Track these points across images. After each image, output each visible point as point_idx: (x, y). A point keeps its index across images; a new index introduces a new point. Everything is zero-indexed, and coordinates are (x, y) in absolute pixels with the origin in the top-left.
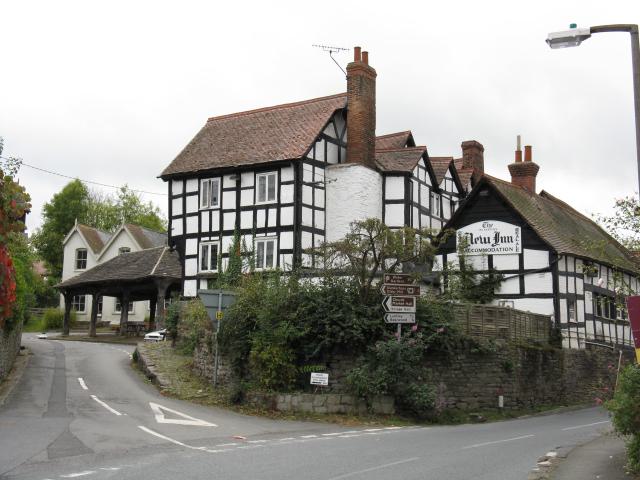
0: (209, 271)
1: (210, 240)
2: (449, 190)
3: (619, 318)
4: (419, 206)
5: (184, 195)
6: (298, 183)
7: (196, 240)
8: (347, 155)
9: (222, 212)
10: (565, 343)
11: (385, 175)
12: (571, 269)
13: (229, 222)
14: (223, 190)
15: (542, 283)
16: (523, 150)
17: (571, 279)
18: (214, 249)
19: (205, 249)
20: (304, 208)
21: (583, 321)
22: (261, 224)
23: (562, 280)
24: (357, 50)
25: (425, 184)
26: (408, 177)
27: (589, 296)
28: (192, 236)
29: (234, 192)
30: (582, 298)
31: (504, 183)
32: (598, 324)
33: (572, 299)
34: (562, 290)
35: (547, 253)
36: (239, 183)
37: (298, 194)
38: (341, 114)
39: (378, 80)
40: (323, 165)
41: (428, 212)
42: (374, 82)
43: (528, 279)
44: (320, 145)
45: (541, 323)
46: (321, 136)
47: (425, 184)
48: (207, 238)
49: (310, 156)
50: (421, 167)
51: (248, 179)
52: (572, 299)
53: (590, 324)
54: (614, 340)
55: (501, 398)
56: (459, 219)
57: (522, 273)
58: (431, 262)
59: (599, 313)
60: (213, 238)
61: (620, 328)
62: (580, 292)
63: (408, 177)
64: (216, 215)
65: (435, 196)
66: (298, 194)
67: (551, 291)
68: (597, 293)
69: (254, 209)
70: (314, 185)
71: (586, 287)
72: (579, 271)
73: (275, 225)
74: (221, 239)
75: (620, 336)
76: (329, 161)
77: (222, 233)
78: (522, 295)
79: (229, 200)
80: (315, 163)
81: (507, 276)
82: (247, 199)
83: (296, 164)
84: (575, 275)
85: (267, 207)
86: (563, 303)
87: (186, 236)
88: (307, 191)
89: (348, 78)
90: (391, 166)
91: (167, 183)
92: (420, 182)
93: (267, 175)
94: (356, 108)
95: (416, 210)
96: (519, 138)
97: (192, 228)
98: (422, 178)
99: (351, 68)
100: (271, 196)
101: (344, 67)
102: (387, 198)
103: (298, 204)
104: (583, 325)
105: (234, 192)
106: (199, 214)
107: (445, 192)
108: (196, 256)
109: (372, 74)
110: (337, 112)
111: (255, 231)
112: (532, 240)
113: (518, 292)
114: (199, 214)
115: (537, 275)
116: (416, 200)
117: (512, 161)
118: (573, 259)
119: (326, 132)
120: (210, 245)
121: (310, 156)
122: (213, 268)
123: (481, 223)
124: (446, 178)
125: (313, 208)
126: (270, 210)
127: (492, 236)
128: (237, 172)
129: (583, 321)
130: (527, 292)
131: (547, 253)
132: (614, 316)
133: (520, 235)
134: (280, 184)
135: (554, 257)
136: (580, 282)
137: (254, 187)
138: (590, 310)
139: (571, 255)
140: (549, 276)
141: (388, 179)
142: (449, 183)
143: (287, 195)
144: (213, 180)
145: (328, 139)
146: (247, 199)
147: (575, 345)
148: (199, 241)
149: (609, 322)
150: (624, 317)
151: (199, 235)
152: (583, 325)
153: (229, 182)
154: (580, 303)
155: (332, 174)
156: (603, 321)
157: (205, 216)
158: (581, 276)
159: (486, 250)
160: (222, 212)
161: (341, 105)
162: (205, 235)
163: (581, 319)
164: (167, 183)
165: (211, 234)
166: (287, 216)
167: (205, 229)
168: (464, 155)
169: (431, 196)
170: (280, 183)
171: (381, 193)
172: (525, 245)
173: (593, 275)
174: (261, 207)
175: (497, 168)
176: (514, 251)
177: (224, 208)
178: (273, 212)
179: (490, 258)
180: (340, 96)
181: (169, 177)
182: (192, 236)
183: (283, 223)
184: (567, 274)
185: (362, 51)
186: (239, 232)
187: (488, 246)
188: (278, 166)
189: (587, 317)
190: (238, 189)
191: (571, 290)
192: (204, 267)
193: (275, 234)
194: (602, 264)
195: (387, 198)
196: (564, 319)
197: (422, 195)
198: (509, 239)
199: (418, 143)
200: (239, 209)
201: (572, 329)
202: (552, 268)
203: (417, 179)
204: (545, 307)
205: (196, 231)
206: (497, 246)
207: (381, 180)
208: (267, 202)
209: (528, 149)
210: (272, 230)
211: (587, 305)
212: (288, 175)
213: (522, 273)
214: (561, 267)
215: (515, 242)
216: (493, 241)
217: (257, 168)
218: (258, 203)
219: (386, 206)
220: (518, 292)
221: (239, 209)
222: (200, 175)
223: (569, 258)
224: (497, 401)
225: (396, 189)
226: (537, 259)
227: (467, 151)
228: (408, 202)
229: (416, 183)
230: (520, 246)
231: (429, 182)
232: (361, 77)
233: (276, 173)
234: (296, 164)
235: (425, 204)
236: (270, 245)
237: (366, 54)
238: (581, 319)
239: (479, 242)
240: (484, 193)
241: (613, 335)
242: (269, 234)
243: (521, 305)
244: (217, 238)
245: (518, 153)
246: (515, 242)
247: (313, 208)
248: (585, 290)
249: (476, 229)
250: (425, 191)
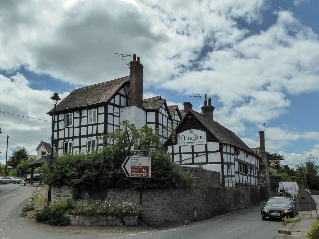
1: (69, 141)
3: (249, 173)
5: (58, 121)
8: (130, 103)
9: (74, 128)
10: (226, 185)
11: (147, 111)
12: (229, 151)
13: (77, 133)
14: (74, 118)
15: (216, 157)
17: (229, 156)
21: (236, 175)
22: (90, 133)
23: (225, 156)
24: (134, 56)
25: (165, 116)
26: (157, 112)
27: (236, 163)
28: (61, 139)
30: (234, 164)
31: (199, 114)
32: (241, 176)
33: (229, 165)
34: (225, 160)
35: (218, 143)
36: (81, 114)
40: (119, 107)
43: (209, 155)
44: (117, 97)
45: (215, 175)
46: (117, 93)
47: (165, 116)
48: (67, 140)
49: (112, 102)
51: (84, 113)
52: (229, 165)
53: (237, 176)
54: (247, 183)
56: (180, 129)
57: (206, 153)
59: (241, 171)
60: (70, 140)
61: (249, 177)
62: (233, 161)
63: (157, 112)
64: (71, 129)
68: (240, 163)
69: (87, 126)
71: (235, 160)
72: (233, 151)
74: (73, 140)
75: (249, 181)
77: (73, 137)
78: (207, 163)
79: (77, 123)
80: (114, 105)
81: (199, 154)
84: (231, 154)
85: (92, 125)
86: (225, 166)
87: (59, 139)
88: (110, 118)
90: (150, 108)
92: (163, 115)
93: (92, 110)
95: (160, 127)
97: (61, 136)
98: (164, 113)
99: (131, 63)
100: (94, 120)
103: (106, 123)
104: (234, 176)
106: (64, 129)
107: (174, 120)
110: (125, 83)
111: (87, 136)
112: (211, 138)
114: (64, 129)
117: (203, 105)
118: (252, 177)
119: (120, 92)
121: (112, 102)
128: (80, 110)
129: (236, 175)
131: (218, 143)
133: (206, 136)
134: (98, 114)
135: (221, 145)
136: (232, 157)
137: (87, 116)
138: (237, 170)
139: (229, 145)
140: (219, 153)
141: (148, 113)
143: (101, 119)
144: (70, 114)
145: (121, 95)
147: (231, 185)
148: (64, 141)
149: (245, 175)
150: (250, 173)
151: (64, 139)
152: (234, 176)
153: (77, 115)
154: (233, 166)
155: (122, 110)
157: (67, 130)
158: (233, 155)
160: (74, 128)
161: (127, 80)
163: (233, 174)
165: (69, 138)
166: (101, 129)
167: (67, 136)
172: (208, 140)
173: (237, 154)
174: (90, 125)
175: (198, 109)
176: (203, 143)
178: (95, 127)
179: (193, 146)
180: (127, 77)
181: (51, 113)
182: (61, 139)
184: (227, 153)
186: (80, 137)
187: (192, 141)
188: (97, 106)
189: (236, 173)
190: (80, 118)
191: (229, 161)
196: (226, 174)
197: (164, 120)
198: (201, 138)
200: (81, 126)
201: (229, 178)
202: (221, 150)
203: (161, 113)
204: (217, 168)
205: (220, 165)
206: (196, 141)
208: (93, 123)
210: (95, 135)
211: (235, 168)
212: (101, 110)
213: (206, 153)
214: (224, 150)
215: (203, 139)
216: (193, 139)
221: (81, 126)
222: (65, 112)
224: (194, 213)
226: (213, 146)
227: (185, 106)
228: (157, 123)
229: (160, 115)
230: (206, 141)
231: (167, 115)
234: (105, 105)
235: (165, 124)
237: (138, 58)
238: (233, 174)
239: (187, 139)
241: (247, 181)
242: (93, 137)
243: (206, 167)
244: (72, 140)
245: (206, 102)
246: (203, 139)
247: (114, 125)
248: (235, 161)
249: (187, 133)
250: (165, 119)
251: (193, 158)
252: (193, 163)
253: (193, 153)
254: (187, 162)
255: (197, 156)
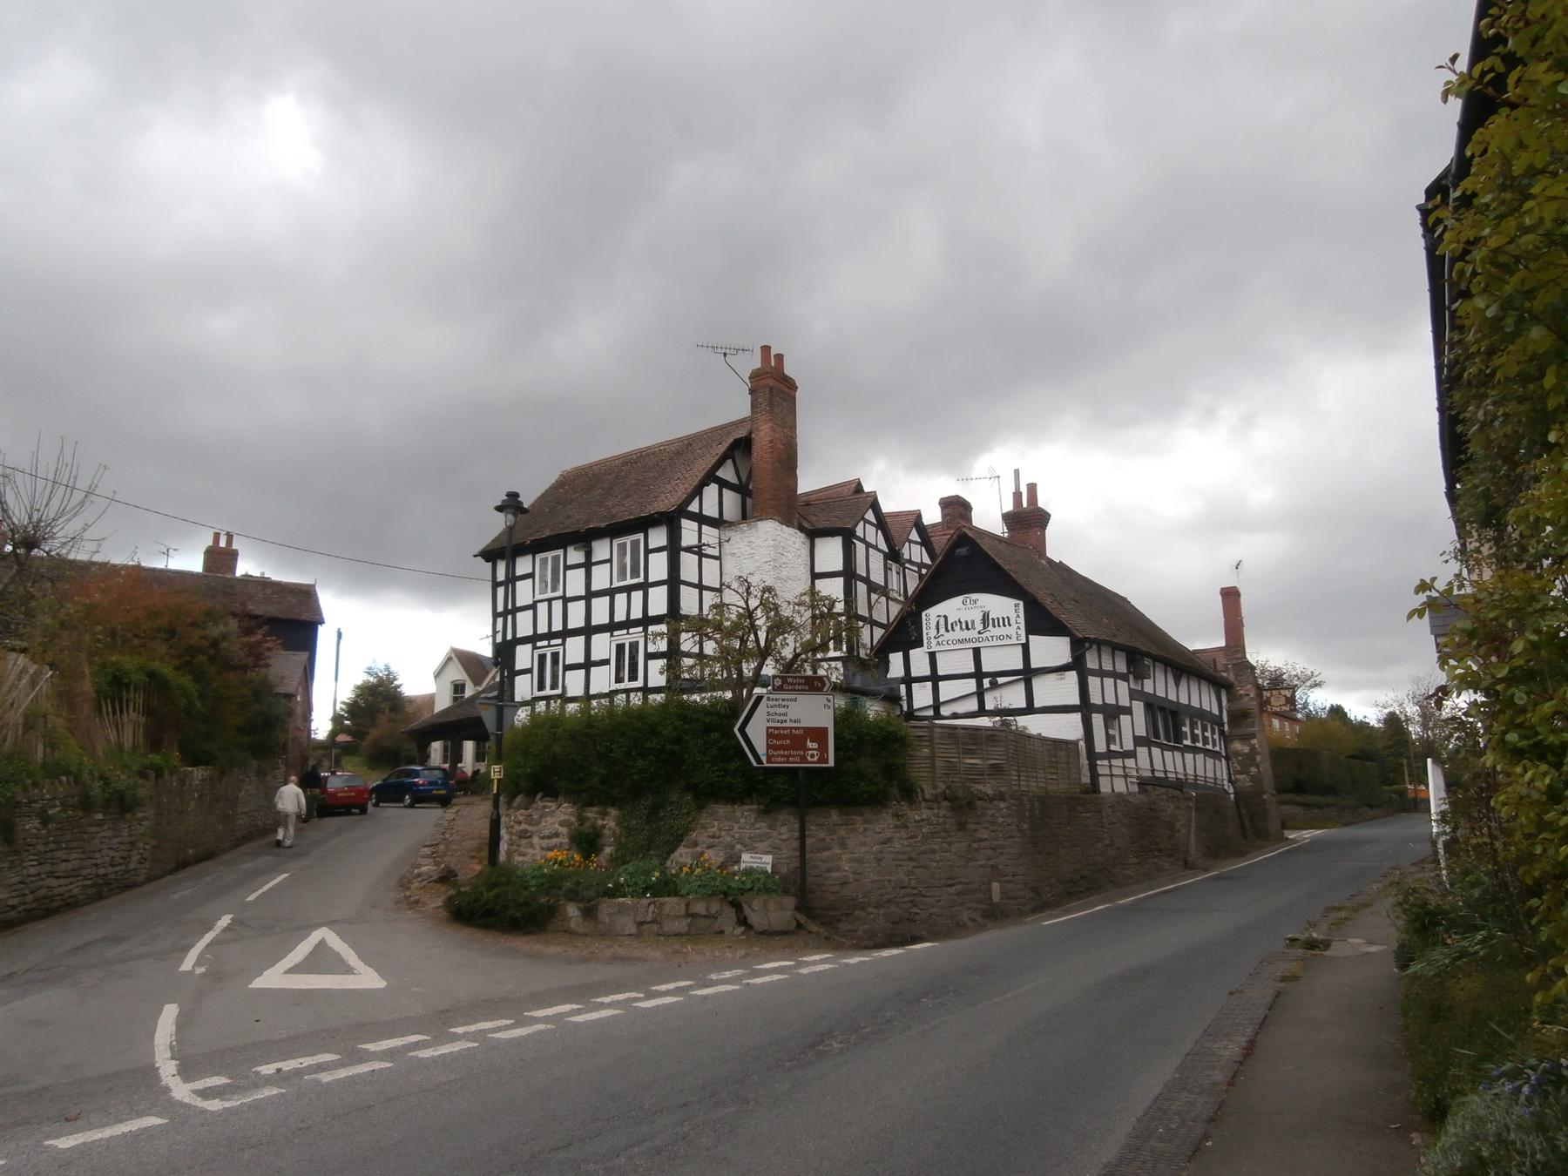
0: (548, 692)
1: (549, 646)
2: (916, 559)
3: (1187, 742)
4: (867, 580)
6: (674, 549)
7: (529, 646)
9: (566, 600)
11: (813, 534)
12: (1107, 666)
15: (1065, 689)
16: (1024, 490)
17: (1109, 682)
18: (555, 656)
19: (542, 658)
20: (683, 587)
22: (620, 616)
23: (1094, 682)
24: (766, 349)
25: (876, 548)
26: (848, 537)
27: (1138, 708)
28: (524, 640)
29: (582, 570)
30: (1128, 711)
32: (1156, 751)
34: (1095, 698)
36: (589, 555)
37: (674, 566)
38: (741, 447)
39: (798, 395)
40: (717, 523)
41: (884, 591)
42: (794, 399)
43: (1039, 684)
44: (711, 491)
47: (876, 548)
48: (545, 643)
49: (694, 507)
50: (916, 543)
51: (601, 549)
52: (1112, 713)
53: (1142, 752)
55: (995, 886)
57: (1028, 674)
58: (886, 665)
59: (1157, 736)
61: (1189, 757)
62: (1124, 701)
63: (848, 537)
64: (557, 606)
65: (894, 566)
66: (674, 566)
67: (1076, 701)
68: (1154, 707)
69: (611, 593)
70: (698, 551)
71: (1133, 695)
73: (641, 616)
74: (563, 644)
76: (726, 517)
77: (566, 633)
78: (1030, 709)
79: (575, 583)
80: (701, 519)
82: (601, 578)
83: (671, 520)
84: (1115, 675)
85: (628, 590)
86: (1098, 720)
88: (688, 562)
89: (752, 392)
90: (821, 525)
91: (490, 564)
92: (868, 545)
94: (764, 436)
95: (861, 588)
96: (1017, 472)
98: (871, 539)
99: (756, 376)
101: (746, 376)
102: (817, 570)
103: (674, 582)
105: (582, 570)
106: (533, 607)
107: (910, 561)
108: (568, 668)
109: (789, 385)
111: (611, 627)
113: (1024, 705)
114: (533, 607)
115: (1053, 676)
116: (861, 571)
117: (1009, 507)
120: (549, 652)
121: (694, 507)
122: (552, 688)
123: (959, 599)
124: (911, 542)
125: (701, 587)
126: (617, 596)
127: (978, 618)
128: (585, 539)
130: (1037, 704)
132: (1179, 737)
134: (648, 551)
135: (1078, 647)
136: (1123, 687)
137: (610, 561)
138: (1141, 731)
140: (1072, 676)
142: (916, 549)
143: (658, 567)
145: (723, 484)
146: (601, 578)
147: (1120, 786)
148: (535, 648)
149: (1172, 749)
151: (533, 639)
153: (575, 556)
154: (1125, 719)
156: (1163, 748)
157: (542, 609)
158: (1124, 678)
159: (969, 640)
161: (742, 433)
162: (601, 629)
164: (490, 564)
166: (658, 602)
168: (944, 516)
169: (887, 569)
170: (648, 551)
171: (809, 563)
172: (1031, 630)
173: (1140, 676)
174: (620, 590)
177: (568, 595)
178: (637, 596)
179: (977, 653)
180: (743, 421)
181: (490, 555)
182: (524, 640)
183: (651, 613)
184: (1101, 673)
185: (773, 352)
187: (973, 634)
188: (643, 525)
189: (1138, 741)
190: (588, 565)
191: (1110, 700)
192: (541, 687)
193: (641, 629)
194: (1155, 659)
195: (817, 570)
196: (1100, 746)
197: (876, 568)
198: (1006, 622)
199: (867, 489)
200: (590, 595)
201: (1114, 762)
202: (1077, 664)
203: (863, 541)
204: (1067, 728)
207: (808, 544)
208: (629, 581)
209: (1032, 488)
210: (636, 623)
211: (1135, 723)
212: (658, 537)
213: (1028, 674)
214: (1091, 662)
215: (1014, 626)
216: (979, 626)
217: (615, 531)
218: (616, 584)
219: (817, 581)
220: (1024, 705)
221: (590, 595)
223: (1103, 648)
225: (830, 553)
226: (1052, 650)
228: (849, 574)
229: (860, 547)
230: (1022, 632)
231: (883, 546)
232: (771, 389)
233: (641, 536)
235: (877, 577)
236: (634, 646)
237: (780, 357)
240: (963, 551)
242: (631, 630)
243: (1035, 725)
244: (559, 641)
245: (1017, 496)
246: (1014, 626)
247: (701, 587)
248: (1132, 698)
249: (952, 608)
250: (877, 561)
251: (980, 694)
252: (982, 711)
253: (978, 674)
254: (961, 708)
255: (994, 686)
